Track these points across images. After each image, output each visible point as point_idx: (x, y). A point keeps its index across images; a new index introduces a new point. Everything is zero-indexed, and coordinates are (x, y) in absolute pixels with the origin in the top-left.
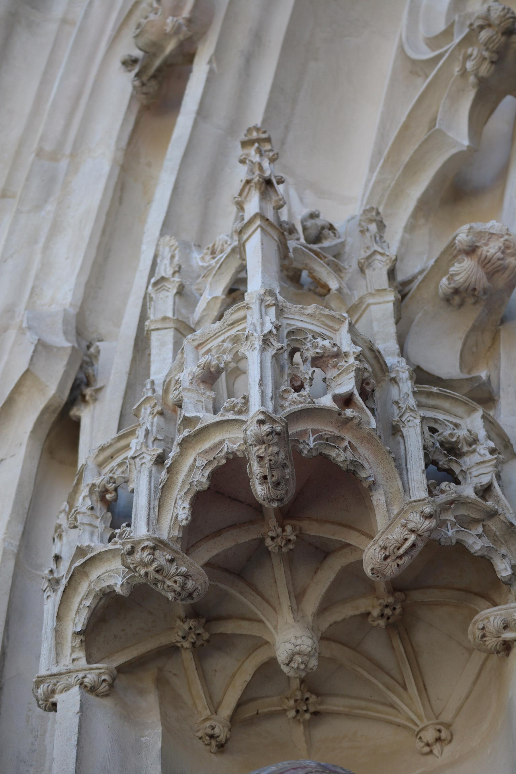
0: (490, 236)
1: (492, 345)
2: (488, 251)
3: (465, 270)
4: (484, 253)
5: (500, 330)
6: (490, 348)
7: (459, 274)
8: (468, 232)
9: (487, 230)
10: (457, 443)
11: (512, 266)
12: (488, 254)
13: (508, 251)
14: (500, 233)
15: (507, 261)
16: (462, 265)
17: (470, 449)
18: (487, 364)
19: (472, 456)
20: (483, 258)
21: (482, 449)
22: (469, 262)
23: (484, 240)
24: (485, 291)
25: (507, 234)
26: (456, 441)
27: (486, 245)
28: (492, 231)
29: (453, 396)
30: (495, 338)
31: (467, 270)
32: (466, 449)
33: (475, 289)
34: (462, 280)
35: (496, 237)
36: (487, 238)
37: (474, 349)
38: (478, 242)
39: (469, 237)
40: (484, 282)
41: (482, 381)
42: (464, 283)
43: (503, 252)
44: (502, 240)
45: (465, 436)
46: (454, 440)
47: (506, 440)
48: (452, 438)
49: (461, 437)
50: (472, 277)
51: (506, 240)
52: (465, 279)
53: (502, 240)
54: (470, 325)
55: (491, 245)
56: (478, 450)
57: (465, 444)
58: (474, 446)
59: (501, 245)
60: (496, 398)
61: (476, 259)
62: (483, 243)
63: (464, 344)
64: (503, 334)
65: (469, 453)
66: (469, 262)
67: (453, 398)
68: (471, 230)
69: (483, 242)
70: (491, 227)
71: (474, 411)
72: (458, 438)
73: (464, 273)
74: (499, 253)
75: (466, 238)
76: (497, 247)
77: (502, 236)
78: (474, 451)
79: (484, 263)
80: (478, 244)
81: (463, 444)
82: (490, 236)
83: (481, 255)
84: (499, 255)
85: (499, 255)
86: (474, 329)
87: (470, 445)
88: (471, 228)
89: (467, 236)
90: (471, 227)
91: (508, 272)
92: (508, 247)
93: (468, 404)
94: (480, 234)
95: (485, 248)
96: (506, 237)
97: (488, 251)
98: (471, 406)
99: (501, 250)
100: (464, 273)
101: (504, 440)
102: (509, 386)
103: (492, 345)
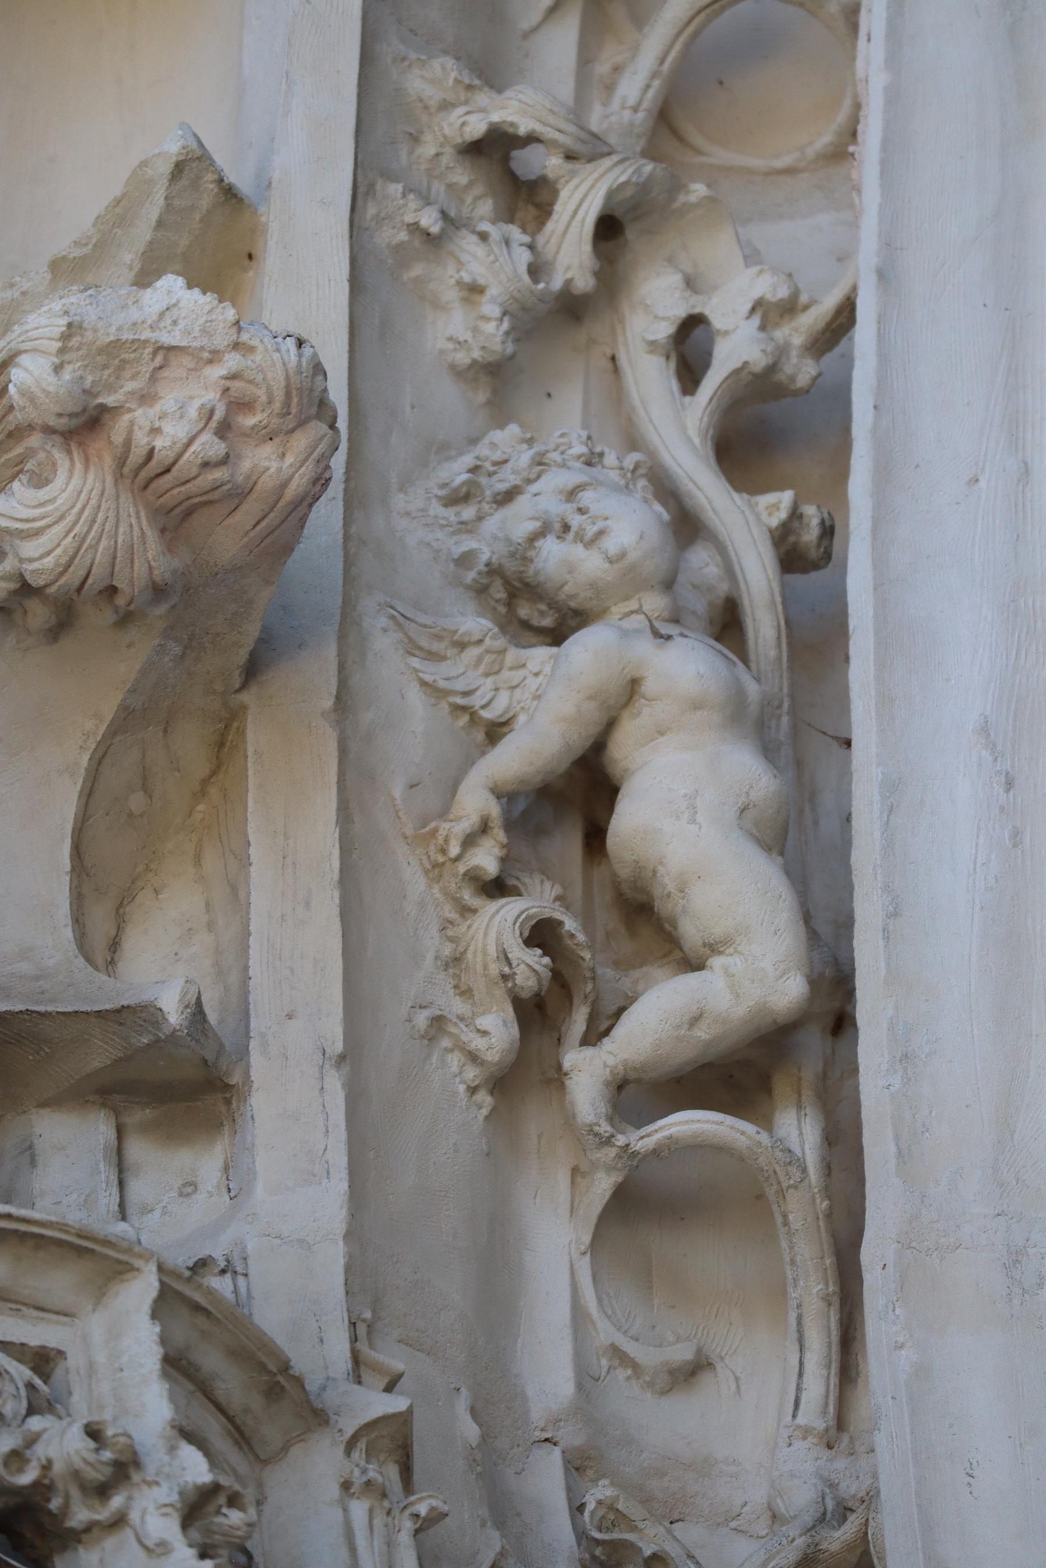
0: (159, 359)
1: (213, 773)
2: (155, 431)
3: (62, 518)
4: (141, 440)
5: (244, 708)
6: (205, 782)
7: (38, 533)
8: (62, 351)
9: (146, 334)
10: (43, 1488)
11: (267, 483)
12: (159, 443)
13: (249, 421)
14: (205, 341)
15: (246, 465)
16: (43, 494)
17: (103, 1514)
18: (198, 860)
19: (110, 1543)
20: (137, 454)
21: (151, 1509)
22: (76, 481)
23: (133, 378)
24: (159, 591)
25: (236, 346)
26: (36, 1484)
27: (146, 398)
28: (166, 339)
29: (23, 1227)
30: (225, 743)
31: (70, 519)
32: (80, 1515)
33: (112, 591)
34: (49, 561)
35: (187, 361)
36: (146, 370)
37: (137, 801)
38: (111, 388)
39: (67, 375)
40: (152, 558)
41: (167, 1031)
42: (61, 574)
43: (224, 430)
44: (216, 372)
45: (79, 1464)
46: (27, 1478)
47: (272, 1367)
48: (21, 1470)
49: (58, 1468)
50: (94, 547)
51: (233, 377)
52: (64, 560)
53: (216, 372)
54: (109, 709)
55: (168, 402)
56: (134, 1516)
57: (75, 1493)
58: (117, 1501)
59: (211, 396)
60: (235, 1079)
61: (108, 461)
62: (132, 393)
63: (88, 795)
64: (257, 736)
65: (96, 1531)
66: (76, 481)
67: (23, 1236)
68: (74, 342)
69: (130, 386)
70: (162, 315)
71: (121, 1273)
72: (47, 1467)
73: (59, 529)
74: (207, 437)
75: (51, 382)
76: (193, 412)
77: (215, 357)
78: (119, 1522)
79: (145, 474)
80: (110, 400)
81: (67, 1498)
82: (159, 359)
83: (128, 443)
84: (208, 445)
85: (208, 445)
86: (126, 721)
87: (102, 1491)
88: (72, 330)
89: (58, 369)
90: (70, 325)
91: (250, 511)
92: (242, 405)
93: (92, 1251)
94: (115, 355)
95: (142, 416)
96: (233, 361)
97: (155, 431)
98: (106, 1257)
99: (213, 424)
100: (59, 529)
101: (263, 1368)
102: (290, 1017)
103: (213, 773)
